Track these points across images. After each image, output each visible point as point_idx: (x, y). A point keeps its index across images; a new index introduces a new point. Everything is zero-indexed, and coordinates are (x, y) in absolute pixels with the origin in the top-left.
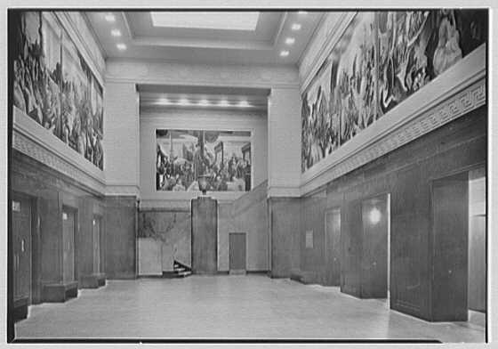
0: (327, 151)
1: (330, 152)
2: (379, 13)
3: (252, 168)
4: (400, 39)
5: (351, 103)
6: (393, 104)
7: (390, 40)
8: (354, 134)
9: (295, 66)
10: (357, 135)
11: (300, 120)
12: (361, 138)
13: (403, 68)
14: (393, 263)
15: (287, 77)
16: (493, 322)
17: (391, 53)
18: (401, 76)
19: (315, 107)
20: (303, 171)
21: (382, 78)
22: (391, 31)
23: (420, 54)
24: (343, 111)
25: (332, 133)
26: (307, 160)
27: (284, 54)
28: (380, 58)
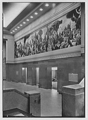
0: (23, 56)
1: (24, 56)
2: (74, 116)
3: (7, 58)
4: (41, 42)
5: (29, 49)
6: (39, 53)
7: (39, 41)
8: (30, 55)
9: (13, 35)
10: (31, 55)
11: (14, 47)
12: (31, 56)
13: (42, 47)
14: (28, 72)
15: (12, 37)
16: (5, 23)
17: (39, 44)
18: (41, 49)
19: (19, 46)
20: (15, 58)
21: (37, 47)
22: (39, 40)
23: (45, 46)
24: (27, 50)
25: (24, 53)
26: (16, 56)
27: (11, 33)
28: (36, 44)
